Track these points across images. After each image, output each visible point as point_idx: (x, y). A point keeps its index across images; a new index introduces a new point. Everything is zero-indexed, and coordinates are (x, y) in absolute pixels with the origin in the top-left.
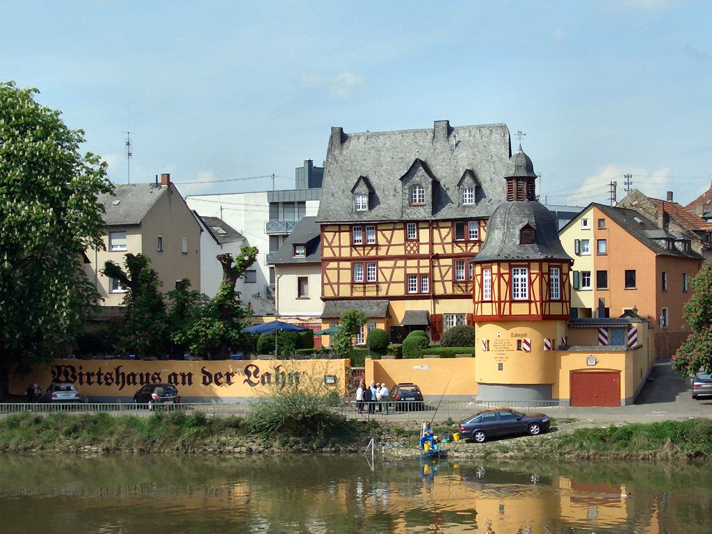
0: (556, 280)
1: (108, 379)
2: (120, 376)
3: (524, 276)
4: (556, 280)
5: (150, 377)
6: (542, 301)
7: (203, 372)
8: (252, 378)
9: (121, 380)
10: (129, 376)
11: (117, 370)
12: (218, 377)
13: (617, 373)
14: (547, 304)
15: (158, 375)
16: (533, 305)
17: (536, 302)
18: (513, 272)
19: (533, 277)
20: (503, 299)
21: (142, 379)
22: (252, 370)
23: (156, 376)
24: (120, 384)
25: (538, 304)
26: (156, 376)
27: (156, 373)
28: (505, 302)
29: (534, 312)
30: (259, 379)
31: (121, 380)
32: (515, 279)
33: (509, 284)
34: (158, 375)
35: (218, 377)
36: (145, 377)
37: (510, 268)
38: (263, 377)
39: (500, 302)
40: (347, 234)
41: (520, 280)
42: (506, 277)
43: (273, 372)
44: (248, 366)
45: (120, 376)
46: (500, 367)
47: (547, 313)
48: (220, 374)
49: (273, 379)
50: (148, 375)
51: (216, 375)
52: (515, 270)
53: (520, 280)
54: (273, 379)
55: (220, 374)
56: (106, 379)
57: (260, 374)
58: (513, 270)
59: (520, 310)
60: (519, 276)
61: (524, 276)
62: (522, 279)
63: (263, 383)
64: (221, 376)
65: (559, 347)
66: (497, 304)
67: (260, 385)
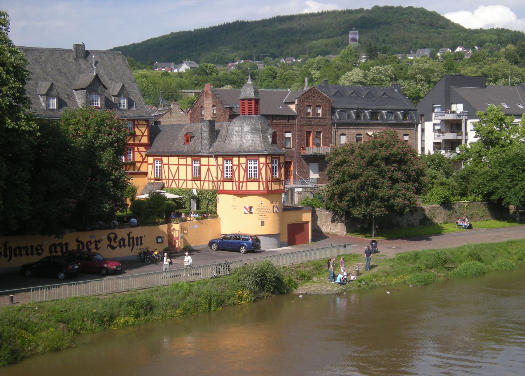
0: (276, 167)
1: (39, 250)
2: (131, 240)
3: (255, 165)
4: (276, 167)
5: (34, 248)
6: (267, 181)
7: (77, 241)
8: (113, 244)
9: (8, 253)
10: (15, 250)
11: (129, 235)
12: (89, 244)
13: (308, 223)
14: (245, 184)
15: (41, 246)
16: (234, 183)
17: (263, 182)
18: (248, 162)
19: (261, 165)
20: (241, 180)
21: (62, 249)
22: (112, 236)
23: (39, 248)
24: (8, 257)
25: (264, 183)
26: (39, 248)
27: (39, 245)
28: (243, 182)
29: (262, 188)
30: (118, 243)
31: (8, 253)
32: (249, 167)
33: (246, 171)
34: (41, 246)
35: (89, 244)
36: (139, 243)
37: (192, 160)
38: (120, 241)
39: (239, 182)
40: (425, 154)
41: (253, 168)
42: (244, 166)
43: (126, 237)
44: (110, 234)
45: (131, 240)
46: (263, 224)
47: (270, 189)
48: (90, 242)
49: (127, 242)
50: (32, 247)
51: (87, 243)
52: (249, 161)
53: (253, 168)
54: (127, 242)
55: (90, 242)
56: (37, 250)
57: (118, 240)
58: (225, 161)
59: (253, 186)
60: (253, 165)
61: (255, 165)
62: (254, 167)
63: (120, 247)
64: (91, 244)
65: (393, 206)
66: (237, 183)
67: (118, 247)
